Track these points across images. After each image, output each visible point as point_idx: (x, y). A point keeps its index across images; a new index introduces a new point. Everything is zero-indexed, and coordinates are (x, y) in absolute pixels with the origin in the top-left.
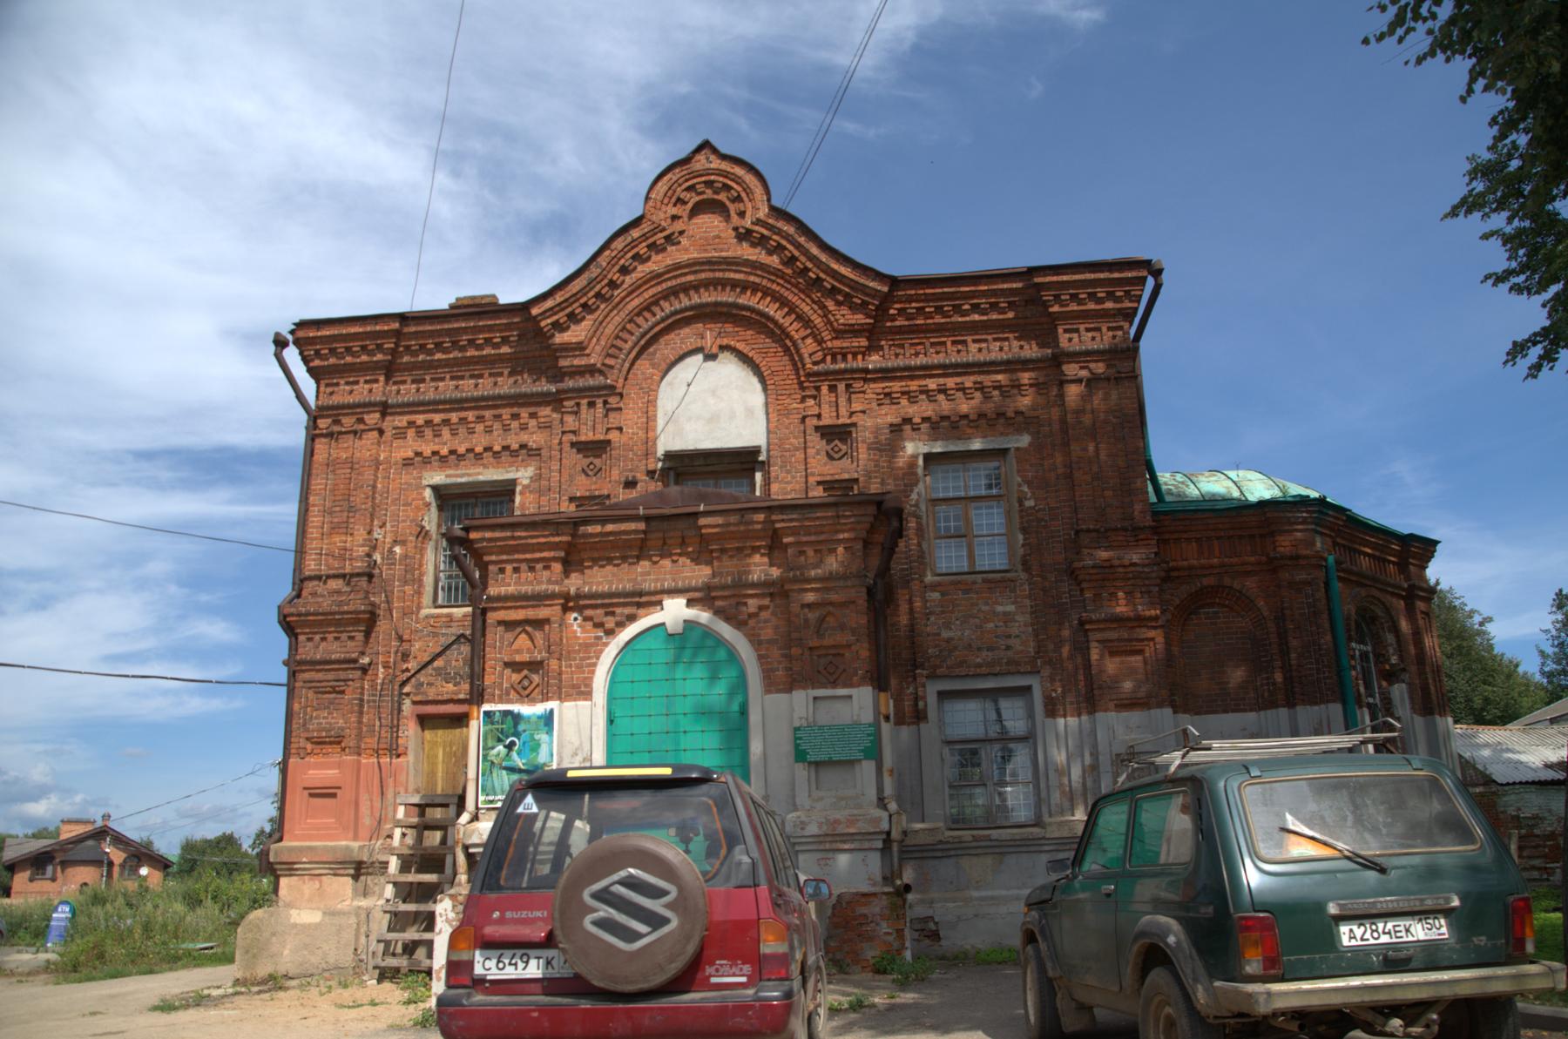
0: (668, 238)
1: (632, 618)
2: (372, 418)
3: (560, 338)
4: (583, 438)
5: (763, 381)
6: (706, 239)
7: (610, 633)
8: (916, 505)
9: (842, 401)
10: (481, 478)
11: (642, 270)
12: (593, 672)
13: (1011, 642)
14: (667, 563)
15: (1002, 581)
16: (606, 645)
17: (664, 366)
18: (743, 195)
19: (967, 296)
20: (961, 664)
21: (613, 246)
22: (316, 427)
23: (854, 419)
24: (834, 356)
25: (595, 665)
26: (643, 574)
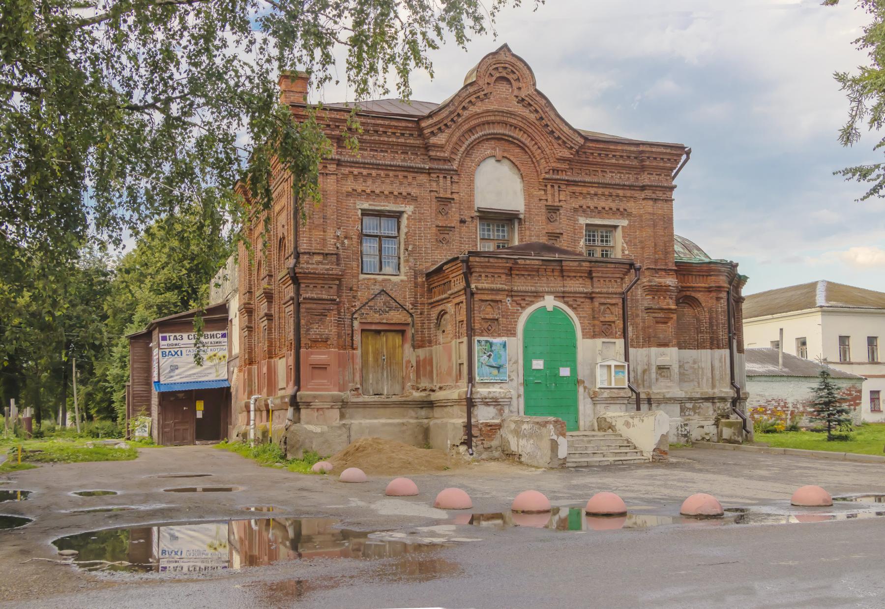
0: (485, 95)
1: (532, 303)
2: (332, 167)
3: (433, 140)
4: (441, 196)
5: (522, 177)
7: (523, 308)
9: (556, 194)
10: (388, 208)
11: (473, 109)
14: (544, 279)
23: (561, 204)
24: (553, 170)
26: (541, 285)
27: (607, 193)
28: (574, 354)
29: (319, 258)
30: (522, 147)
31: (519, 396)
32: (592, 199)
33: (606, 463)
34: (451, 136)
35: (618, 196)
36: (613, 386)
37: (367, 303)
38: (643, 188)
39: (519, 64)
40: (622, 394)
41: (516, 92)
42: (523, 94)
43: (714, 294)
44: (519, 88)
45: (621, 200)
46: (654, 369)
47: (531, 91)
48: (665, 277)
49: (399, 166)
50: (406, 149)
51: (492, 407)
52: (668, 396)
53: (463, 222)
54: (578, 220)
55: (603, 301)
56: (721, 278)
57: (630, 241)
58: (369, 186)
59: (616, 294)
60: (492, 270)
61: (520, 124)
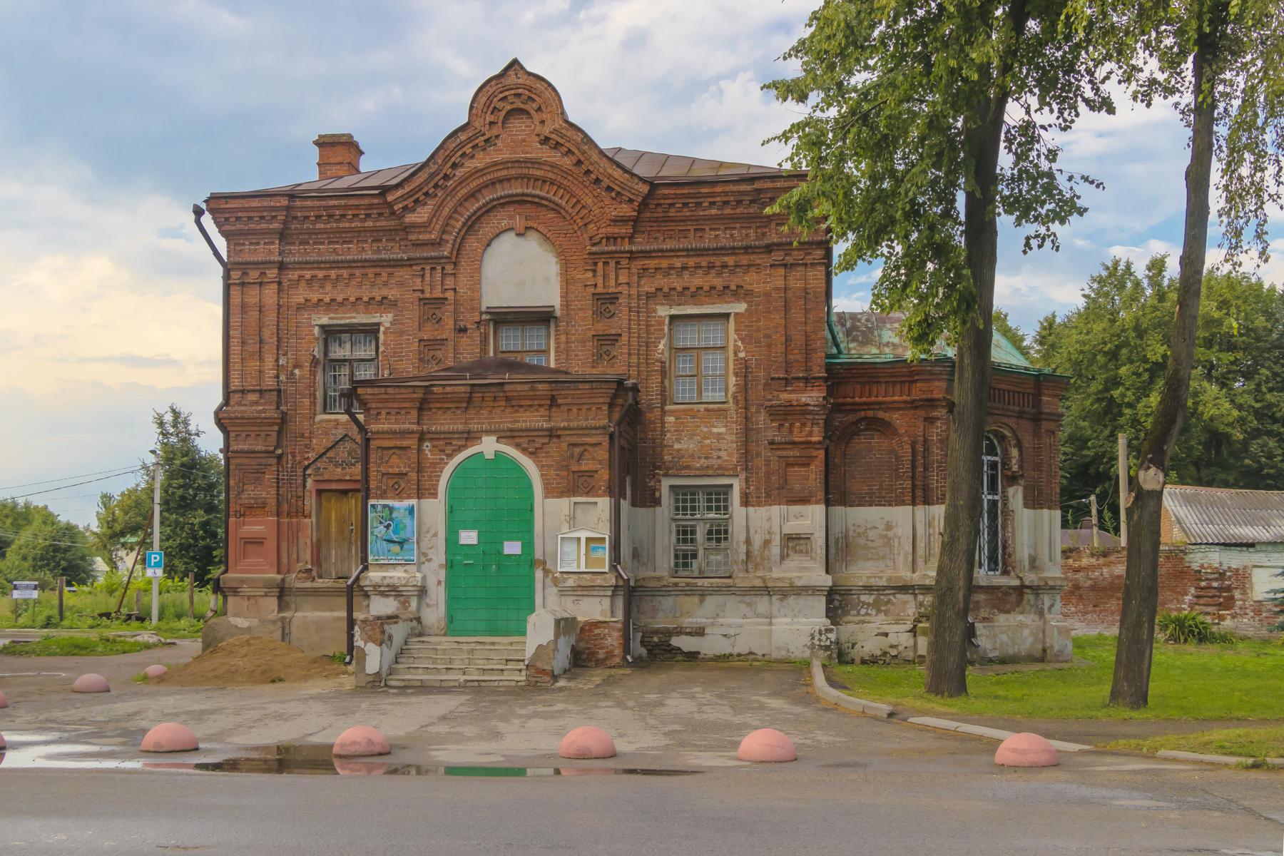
0: (487, 141)
1: (460, 449)
3: (410, 218)
4: (428, 295)
7: (450, 456)
10: (355, 321)
11: (470, 165)
15: (719, 410)
17: (486, 242)
18: (543, 107)
19: (705, 196)
23: (620, 289)
24: (608, 239)
27: (704, 264)
28: (530, 522)
29: (253, 397)
30: (556, 209)
31: (439, 583)
32: (679, 275)
33: (452, 684)
35: (724, 266)
36: (583, 569)
37: (324, 453)
38: (769, 248)
39: (539, 86)
40: (599, 581)
41: (538, 128)
42: (546, 131)
43: (922, 413)
44: (543, 122)
45: (732, 272)
46: (776, 540)
47: (559, 124)
48: (803, 391)
49: (370, 261)
50: (377, 235)
51: (391, 599)
52: (799, 583)
53: (463, 330)
54: (655, 311)
55: (575, 440)
56: (936, 383)
57: (751, 337)
59: (596, 428)
61: (550, 175)
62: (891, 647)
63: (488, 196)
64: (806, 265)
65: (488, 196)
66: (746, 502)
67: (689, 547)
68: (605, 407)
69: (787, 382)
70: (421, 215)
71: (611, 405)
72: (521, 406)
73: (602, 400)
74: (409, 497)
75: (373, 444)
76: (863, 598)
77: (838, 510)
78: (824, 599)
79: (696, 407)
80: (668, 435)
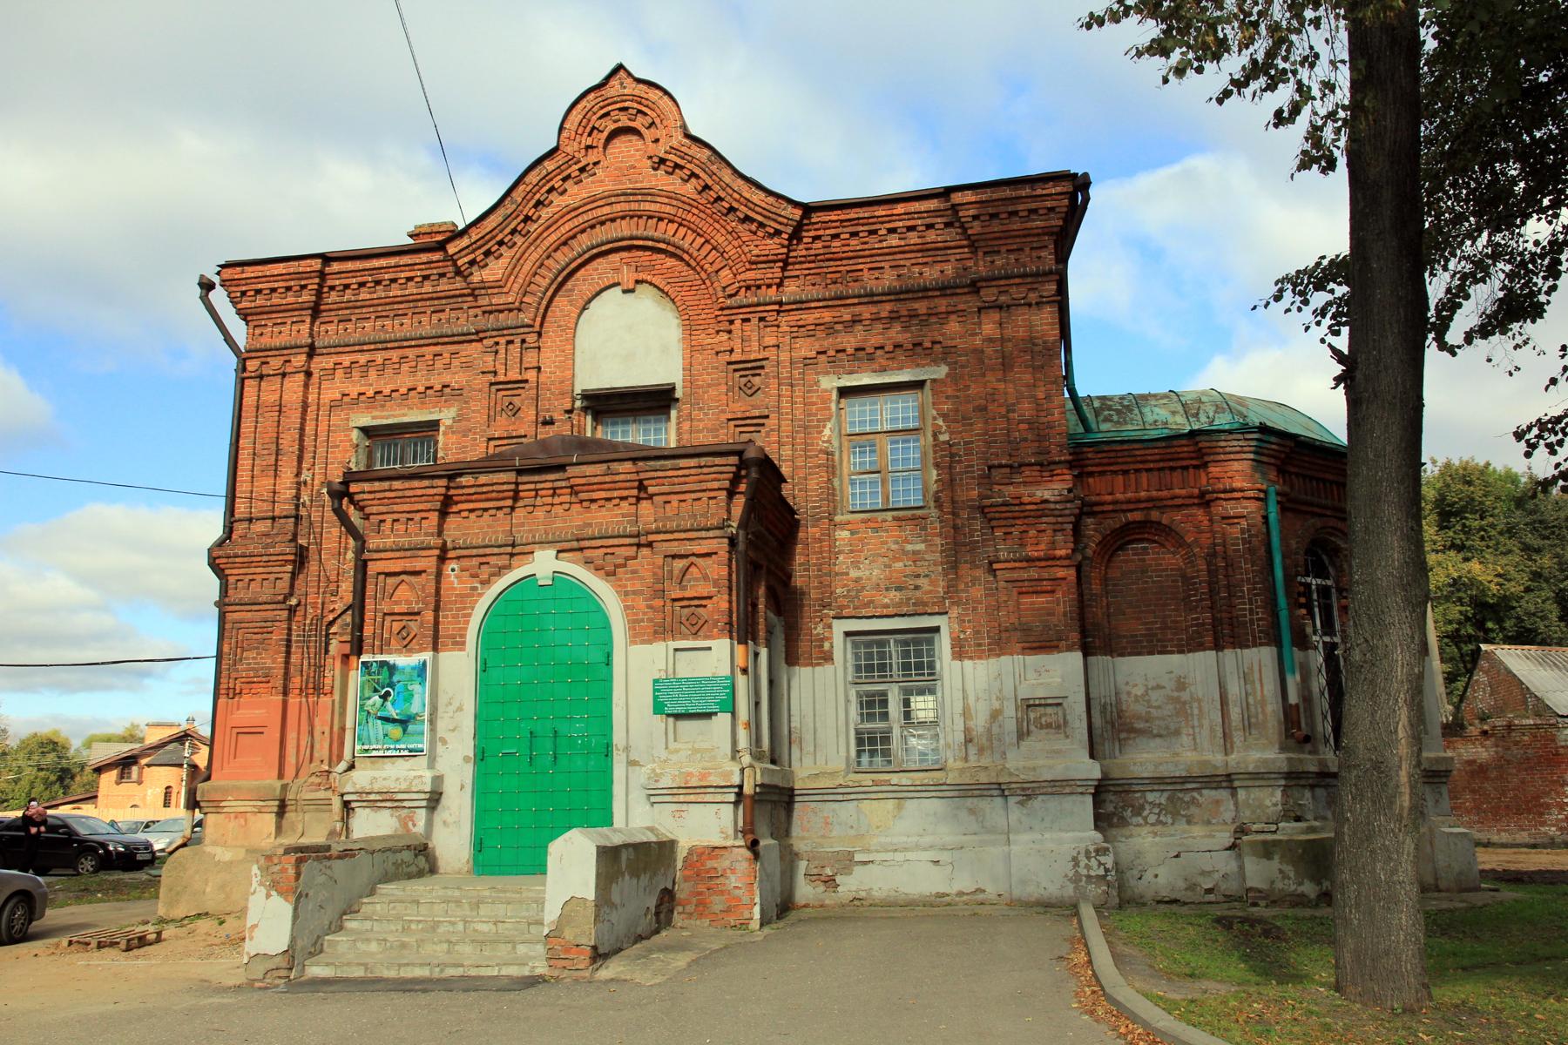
0: (582, 170)
1: (500, 571)
4: (501, 378)
6: (620, 168)
7: (486, 583)
8: (829, 441)
11: (558, 201)
12: (467, 622)
13: (920, 582)
15: (914, 518)
16: (481, 595)
17: (581, 303)
18: (657, 121)
20: (867, 605)
21: (527, 180)
22: (244, 369)
25: (470, 615)
26: (525, 522)
34: (518, 261)
35: (913, 315)
42: (661, 151)
50: (439, 301)
54: (817, 383)
55: (675, 548)
56: (1236, 466)
58: (373, 383)
60: (406, 507)
61: (668, 209)
62: (1203, 873)
63: (585, 240)
64: (1030, 305)
65: (585, 240)
66: (959, 653)
67: (879, 725)
68: (723, 495)
69: (1015, 468)
70: (494, 270)
71: (731, 494)
72: (593, 501)
73: (716, 485)
74: (421, 650)
75: (372, 568)
76: (1150, 797)
77: (1099, 661)
78: (1089, 800)
79: (880, 516)
80: (841, 558)
